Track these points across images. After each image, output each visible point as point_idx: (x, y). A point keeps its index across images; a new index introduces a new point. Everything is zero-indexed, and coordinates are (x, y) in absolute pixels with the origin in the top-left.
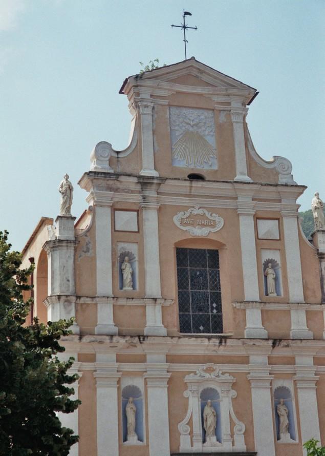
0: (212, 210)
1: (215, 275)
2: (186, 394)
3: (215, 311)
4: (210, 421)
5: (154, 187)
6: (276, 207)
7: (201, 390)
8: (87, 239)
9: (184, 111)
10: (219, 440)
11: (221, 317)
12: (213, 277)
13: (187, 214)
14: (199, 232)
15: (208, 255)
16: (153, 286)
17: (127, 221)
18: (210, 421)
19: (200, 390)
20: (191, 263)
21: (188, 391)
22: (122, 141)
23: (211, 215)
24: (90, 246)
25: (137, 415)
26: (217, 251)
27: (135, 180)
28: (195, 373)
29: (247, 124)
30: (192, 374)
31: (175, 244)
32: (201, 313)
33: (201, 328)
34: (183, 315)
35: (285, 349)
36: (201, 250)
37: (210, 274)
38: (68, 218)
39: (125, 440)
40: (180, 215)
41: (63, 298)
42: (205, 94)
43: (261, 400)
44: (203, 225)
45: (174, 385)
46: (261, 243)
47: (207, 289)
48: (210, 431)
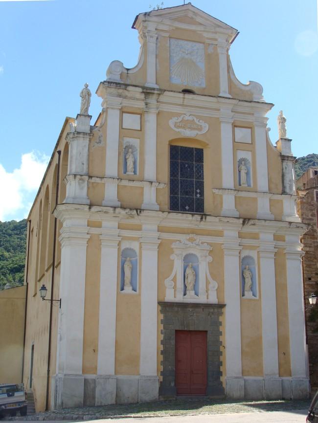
0: (199, 118)
2: (172, 257)
3: (198, 195)
4: (190, 279)
6: (250, 119)
8: (100, 134)
9: (181, 42)
10: (197, 294)
11: (203, 201)
12: (198, 169)
13: (180, 119)
14: (188, 133)
15: (195, 152)
17: (131, 122)
22: (131, 61)
26: (202, 150)
30: (178, 242)
31: (170, 142)
32: (187, 196)
33: (187, 208)
34: (172, 197)
35: (252, 227)
37: (196, 167)
39: (122, 289)
40: (175, 119)
41: (78, 177)
43: (231, 267)
44: (191, 129)
45: (164, 250)
46: (237, 145)
48: (189, 287)
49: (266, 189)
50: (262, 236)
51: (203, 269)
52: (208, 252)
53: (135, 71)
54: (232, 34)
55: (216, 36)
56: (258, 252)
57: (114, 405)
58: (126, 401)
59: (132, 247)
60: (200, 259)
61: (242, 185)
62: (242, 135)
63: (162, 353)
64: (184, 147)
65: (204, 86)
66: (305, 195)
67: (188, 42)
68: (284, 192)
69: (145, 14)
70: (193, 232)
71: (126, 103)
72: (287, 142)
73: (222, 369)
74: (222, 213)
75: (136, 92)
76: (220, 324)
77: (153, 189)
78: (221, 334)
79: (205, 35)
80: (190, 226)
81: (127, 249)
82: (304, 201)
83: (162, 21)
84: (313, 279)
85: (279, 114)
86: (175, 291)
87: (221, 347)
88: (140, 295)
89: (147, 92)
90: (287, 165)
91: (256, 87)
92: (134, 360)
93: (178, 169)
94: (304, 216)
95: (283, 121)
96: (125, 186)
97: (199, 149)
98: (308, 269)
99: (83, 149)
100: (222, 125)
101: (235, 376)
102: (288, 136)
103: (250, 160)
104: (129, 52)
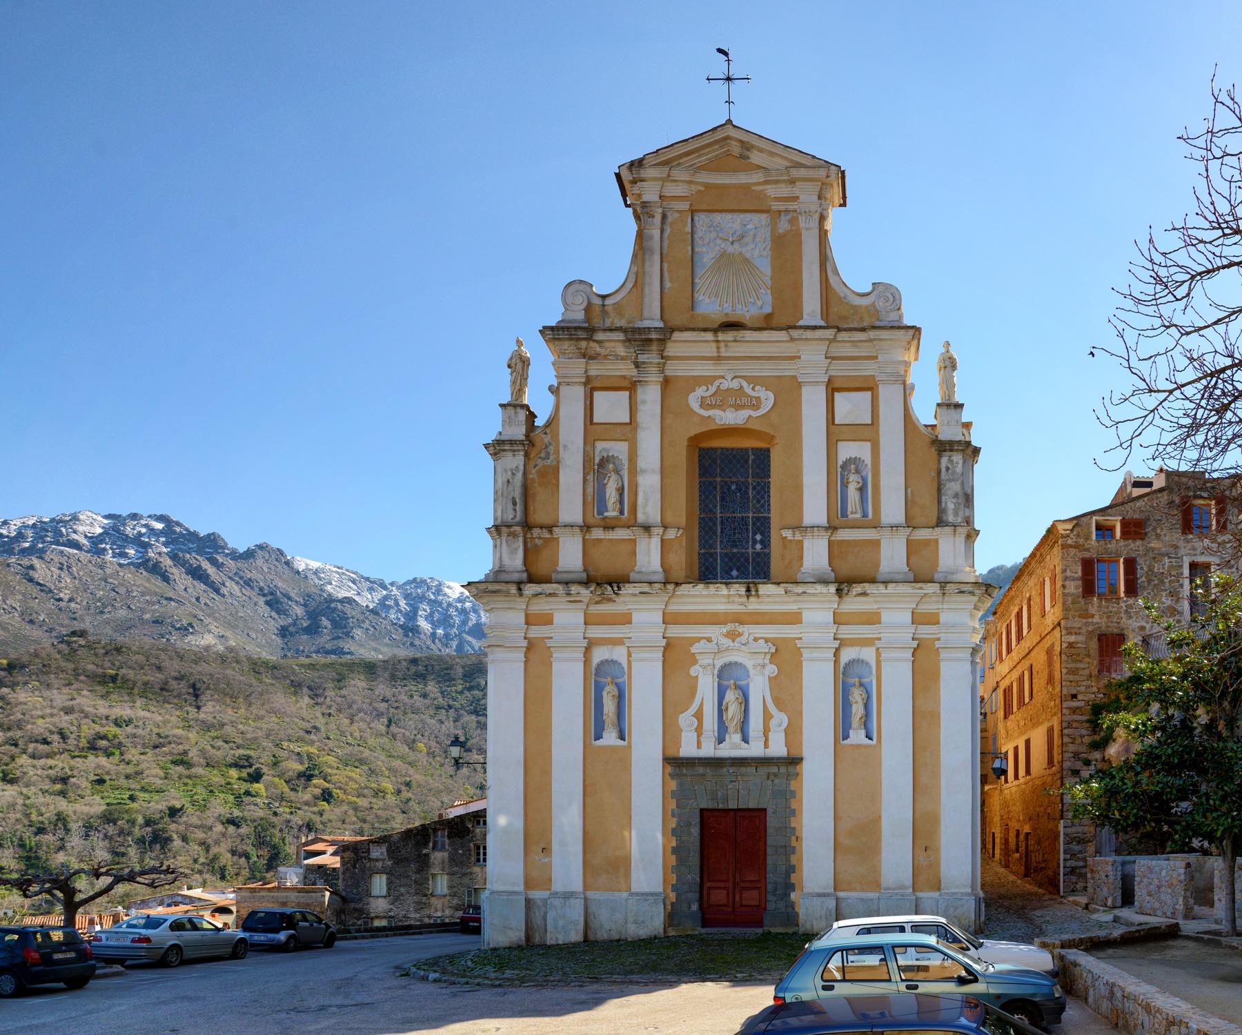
0: (754, 381)
1: (763, 488)
2: (693, 671)
3: (758, 546)
4: (733, 710)
5: (654, 347)
6: (868, 369)
7: (719, 663)
8: (547, 439)
9: (718, 217)
10: (745, 740)
11: (768, 556)
12: (758, 493)
13: (713, 389)
14: (730, 417)
15: (752, 457)
16: (649, 509)
17: (611, 407)
18: (733, 710)
19: (718, 666)
20: (722, 470)
21: (697, 667)
23: (753, 389)
24: (551, 449)
25: (621, 698)
26: (768, 450)
27: (621, 336)
28: (709, 640)
29: (826, 232)
30: (703, 641)
31: (691, 439)
32: (735, 551)
33: (735, 573)
34: (704, 554)
35: (862, 599)
36: (741, 449)
37: (754, 488)
38: (515, 406)
39: (846, 737)
40: (701, 391)
41: (504, 530)
42: (755, 184)
43: (818, 681)
44: (738, 407)
45: (675, 657)
46: (835, 432)
47: (747, 511)
48: (732, 726)
49: (901, 519)
50: (885, 617)
51: (759, 689)
52: (768, 656)
53: (618, 297)
54: (830, 180)
55: (796, 190)
56: (878, 649)
57: (519, 947)
58: (606, 937)
59: (615, 658)
60: (752, 672)
61: (851, 516)
62: (851, 407)
63: (675, 851)
64: (727, 449)
65: (768, 309)
66: (1072, 530)
67: (735, 215)
68: (940, 522)
69: (632, 164)
70: (740, 619)
71: (596, 369)
72: (952, 412)
73: (794, 878)
74: (800, 577)
75: (614, 344)
76: (794, 794)
77: (655, 543)
78: (793, 813)
79: (771, 191)
80: (729, 607)
81: (603, 663)
82: (1070, 542)
83: (669, 176)
84: (1080, 697)
85: (943, 350)
86: (699, 736)
87: (793, 838)
88: (630, 746)
89: (639, 338)
90: (950, 461)
91: (888, 294)
92: (620, 866)
93: (715, 496)
94: (1068, 573)
95: (949, 364)
96: (601, 540)
97: (761, 449)
98: (1071, 677)
99: (513, 474)
100: (806, 391)
101: (820, 891)
102: (958, 398)
103: (868, 461)
104: (605, 252)
